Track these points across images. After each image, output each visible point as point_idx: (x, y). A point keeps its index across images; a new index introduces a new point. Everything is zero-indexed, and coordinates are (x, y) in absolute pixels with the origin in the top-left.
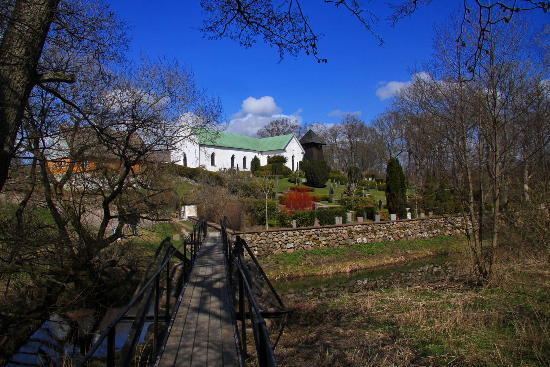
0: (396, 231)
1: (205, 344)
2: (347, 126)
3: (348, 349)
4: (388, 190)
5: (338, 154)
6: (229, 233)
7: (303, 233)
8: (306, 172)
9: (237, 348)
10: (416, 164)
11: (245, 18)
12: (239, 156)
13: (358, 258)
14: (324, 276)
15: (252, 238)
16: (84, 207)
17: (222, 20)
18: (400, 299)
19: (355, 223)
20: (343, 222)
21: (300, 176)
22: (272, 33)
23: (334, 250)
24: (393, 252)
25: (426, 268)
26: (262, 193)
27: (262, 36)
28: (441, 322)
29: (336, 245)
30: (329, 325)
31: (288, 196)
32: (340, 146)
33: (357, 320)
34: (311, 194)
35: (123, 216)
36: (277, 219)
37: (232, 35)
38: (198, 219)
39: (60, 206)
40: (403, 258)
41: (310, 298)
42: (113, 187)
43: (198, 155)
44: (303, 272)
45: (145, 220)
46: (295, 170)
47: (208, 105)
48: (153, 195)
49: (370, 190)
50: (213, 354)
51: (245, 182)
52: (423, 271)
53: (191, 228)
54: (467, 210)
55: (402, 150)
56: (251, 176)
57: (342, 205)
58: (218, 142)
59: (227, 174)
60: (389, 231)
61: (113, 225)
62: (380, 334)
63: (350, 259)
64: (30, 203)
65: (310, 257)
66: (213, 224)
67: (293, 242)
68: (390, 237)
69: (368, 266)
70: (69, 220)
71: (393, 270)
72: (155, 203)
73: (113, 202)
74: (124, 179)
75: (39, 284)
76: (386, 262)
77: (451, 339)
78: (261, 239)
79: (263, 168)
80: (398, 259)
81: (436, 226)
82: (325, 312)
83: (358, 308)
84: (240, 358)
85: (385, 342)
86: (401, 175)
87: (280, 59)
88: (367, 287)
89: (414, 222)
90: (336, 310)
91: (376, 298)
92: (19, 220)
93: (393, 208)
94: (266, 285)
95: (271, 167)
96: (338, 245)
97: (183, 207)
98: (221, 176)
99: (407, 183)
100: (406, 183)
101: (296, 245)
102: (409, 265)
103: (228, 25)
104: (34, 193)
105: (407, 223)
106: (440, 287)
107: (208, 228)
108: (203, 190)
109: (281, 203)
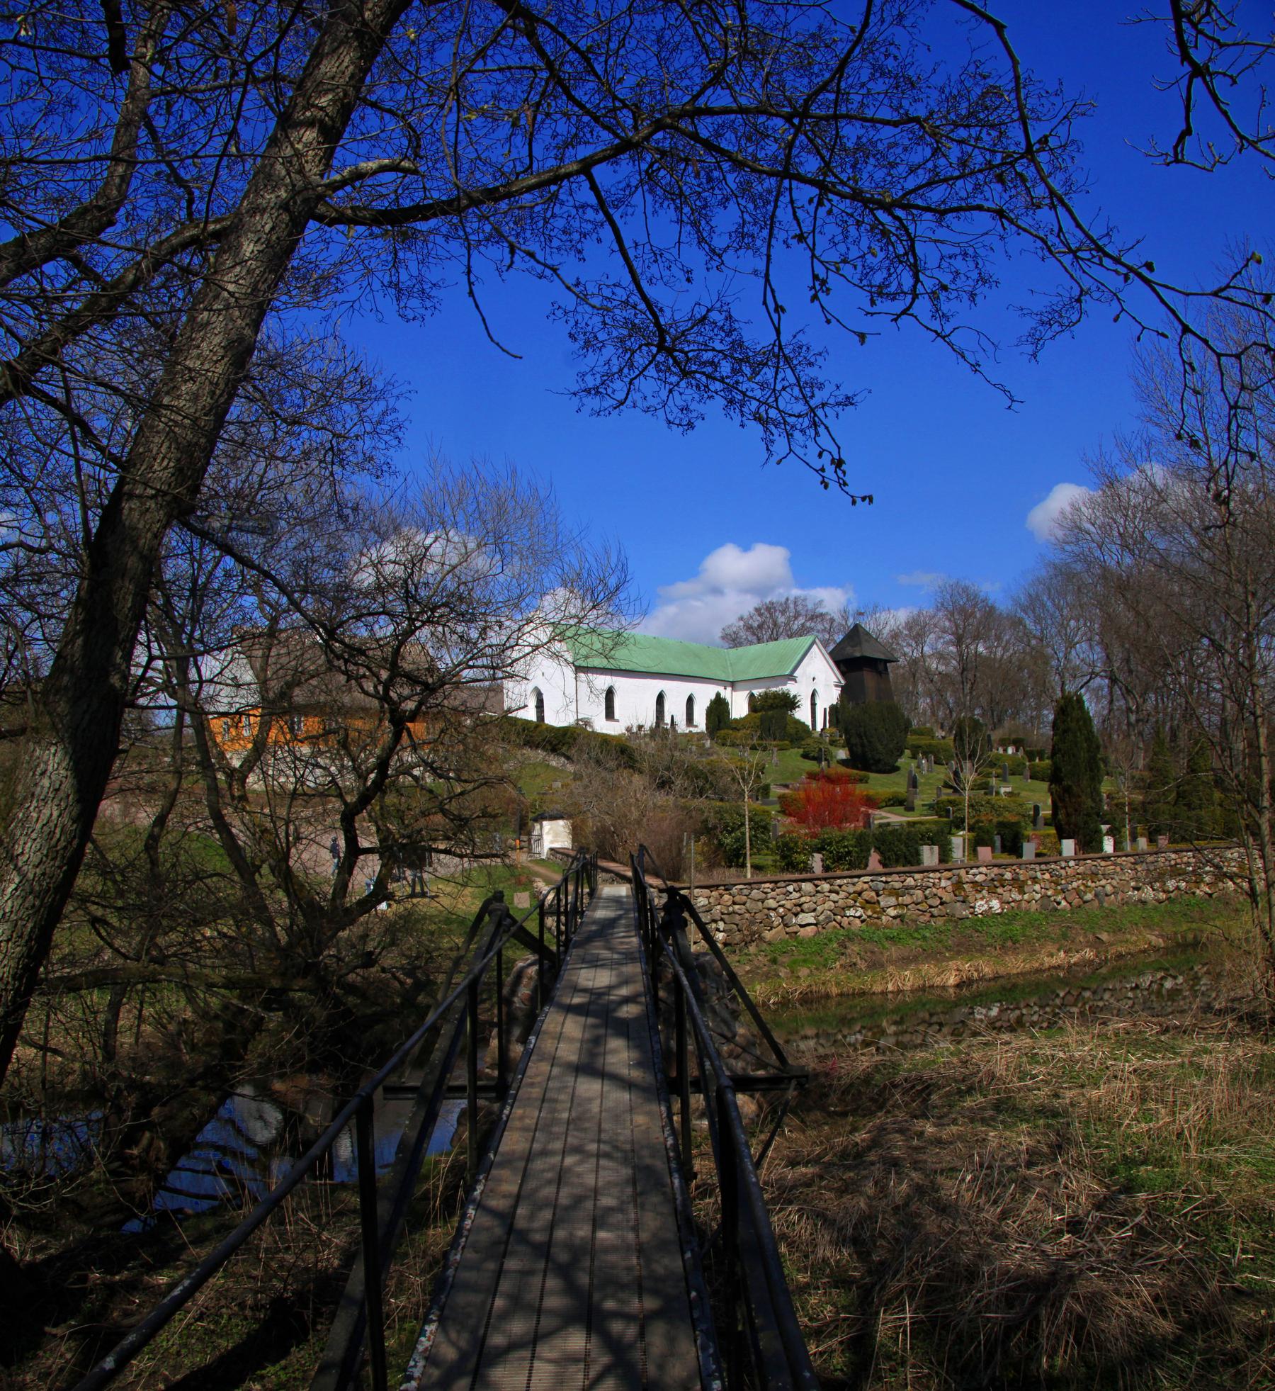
0: (1075, 884)
1: (593, 1147)
2: (952, 614)
3: (942, 1171)
4: (1054, 777)
5: (930, 686)
6: (651, 886)
8: (847, 732)
9: (668, 1158)
10: (1129, 710)
11: (676, 363)
12: (676, 693)
13: (977, 951)
14: (890, 996)
15: (712, 900)
16: (296, 830)
17: (621, 370)
18: (1077, 1054)
19: (972, 863)
20: (941, 861)
21: (833, 743)
22: (744, 394)
23: (916, 930)
24: (1064, 936)
25: (1146, 981)
26: (735, 787)
27: (720, 402)
28: (1174, 1113)
29: (922, 919)
30: (901, 1115)
31: (802, 794)
32: (934, 666)
33: (968, 1102)
34: (860, 789)
35: (390, 848)
36: (773, 853)
37: (646, 404)
38: (573, 853)
39: (242, 828)
40: (1089, 954)
41: (856, 1050)
42: (362, 777)
43: (571, 691)
44: (838, 984)
45: (442, 856)
46: (819, 727)
47: (594, 564)
48: (462, 794)
49: (1010, 778)
50: (613, 1172)
51: (691, 758)
52: (1137, 987)
53: (558, 877)
54: (1255, 832)
55: (1093, 673)
56: (708, 744)
57: (940, 816)
58: (623, 657)
59: (647, 740)
60: (1057, 884)
61: (367, 872)
62: (1022, 1138)
63: (958, 953)
64: (172, 819)
65: (856, 948)
66: (612, 865)
67: (814, 910)
68: (1059, 898)
69: (1002, 971)
70: (263, 862)
71: (1064, 982)
72: (466, 813)
73: (365, 813)
74: (389, 757)
75: (205, 1015)
76: (1048, 962)
77: (1193, 1154)
78: (734, 903)
80: (1078, 956)
81: (1176, 872)
82: (892, 1083)
83: (975, 1074)
84: (676, 1182)
85: (1034, 1159)
86: (1090, 737)
87: (765, 454)
88: (998, 1024)
89: (1119, 860)
90: (920, 1079)
91: (1020, 1049)
92: (154, 862)
93: (1068, 823)
94: (746, 1017)
95: (758, 721)
96: (927, 917)
97: (537, 826)
98: (633, 744)
99: (1105, 761)
100: (1101, 759)
101: (821, 918)
102: (1104, 971)
103: (636, 382)
104: (181, 798)
105: (1103, 863)
106: (1176, 1027)
107: (601, 876)
108: (586, 781)
109: (783, 812)
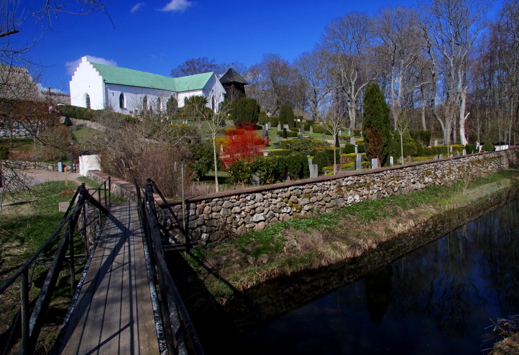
0: (390, 183)
7: (277, 194)
60: (383, 183)
79: (179, 110)
101: (267, 216)
105: (400, 171)
